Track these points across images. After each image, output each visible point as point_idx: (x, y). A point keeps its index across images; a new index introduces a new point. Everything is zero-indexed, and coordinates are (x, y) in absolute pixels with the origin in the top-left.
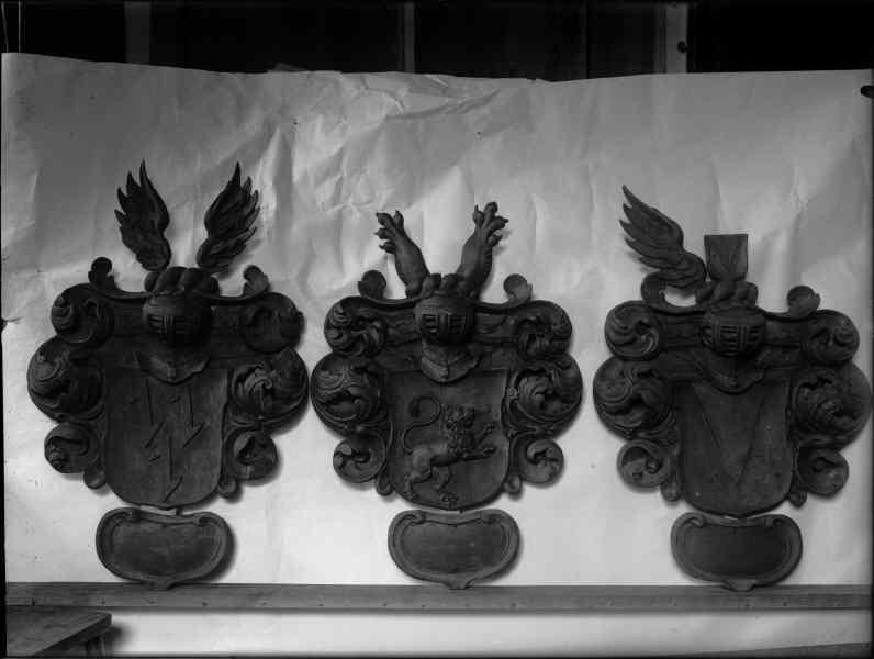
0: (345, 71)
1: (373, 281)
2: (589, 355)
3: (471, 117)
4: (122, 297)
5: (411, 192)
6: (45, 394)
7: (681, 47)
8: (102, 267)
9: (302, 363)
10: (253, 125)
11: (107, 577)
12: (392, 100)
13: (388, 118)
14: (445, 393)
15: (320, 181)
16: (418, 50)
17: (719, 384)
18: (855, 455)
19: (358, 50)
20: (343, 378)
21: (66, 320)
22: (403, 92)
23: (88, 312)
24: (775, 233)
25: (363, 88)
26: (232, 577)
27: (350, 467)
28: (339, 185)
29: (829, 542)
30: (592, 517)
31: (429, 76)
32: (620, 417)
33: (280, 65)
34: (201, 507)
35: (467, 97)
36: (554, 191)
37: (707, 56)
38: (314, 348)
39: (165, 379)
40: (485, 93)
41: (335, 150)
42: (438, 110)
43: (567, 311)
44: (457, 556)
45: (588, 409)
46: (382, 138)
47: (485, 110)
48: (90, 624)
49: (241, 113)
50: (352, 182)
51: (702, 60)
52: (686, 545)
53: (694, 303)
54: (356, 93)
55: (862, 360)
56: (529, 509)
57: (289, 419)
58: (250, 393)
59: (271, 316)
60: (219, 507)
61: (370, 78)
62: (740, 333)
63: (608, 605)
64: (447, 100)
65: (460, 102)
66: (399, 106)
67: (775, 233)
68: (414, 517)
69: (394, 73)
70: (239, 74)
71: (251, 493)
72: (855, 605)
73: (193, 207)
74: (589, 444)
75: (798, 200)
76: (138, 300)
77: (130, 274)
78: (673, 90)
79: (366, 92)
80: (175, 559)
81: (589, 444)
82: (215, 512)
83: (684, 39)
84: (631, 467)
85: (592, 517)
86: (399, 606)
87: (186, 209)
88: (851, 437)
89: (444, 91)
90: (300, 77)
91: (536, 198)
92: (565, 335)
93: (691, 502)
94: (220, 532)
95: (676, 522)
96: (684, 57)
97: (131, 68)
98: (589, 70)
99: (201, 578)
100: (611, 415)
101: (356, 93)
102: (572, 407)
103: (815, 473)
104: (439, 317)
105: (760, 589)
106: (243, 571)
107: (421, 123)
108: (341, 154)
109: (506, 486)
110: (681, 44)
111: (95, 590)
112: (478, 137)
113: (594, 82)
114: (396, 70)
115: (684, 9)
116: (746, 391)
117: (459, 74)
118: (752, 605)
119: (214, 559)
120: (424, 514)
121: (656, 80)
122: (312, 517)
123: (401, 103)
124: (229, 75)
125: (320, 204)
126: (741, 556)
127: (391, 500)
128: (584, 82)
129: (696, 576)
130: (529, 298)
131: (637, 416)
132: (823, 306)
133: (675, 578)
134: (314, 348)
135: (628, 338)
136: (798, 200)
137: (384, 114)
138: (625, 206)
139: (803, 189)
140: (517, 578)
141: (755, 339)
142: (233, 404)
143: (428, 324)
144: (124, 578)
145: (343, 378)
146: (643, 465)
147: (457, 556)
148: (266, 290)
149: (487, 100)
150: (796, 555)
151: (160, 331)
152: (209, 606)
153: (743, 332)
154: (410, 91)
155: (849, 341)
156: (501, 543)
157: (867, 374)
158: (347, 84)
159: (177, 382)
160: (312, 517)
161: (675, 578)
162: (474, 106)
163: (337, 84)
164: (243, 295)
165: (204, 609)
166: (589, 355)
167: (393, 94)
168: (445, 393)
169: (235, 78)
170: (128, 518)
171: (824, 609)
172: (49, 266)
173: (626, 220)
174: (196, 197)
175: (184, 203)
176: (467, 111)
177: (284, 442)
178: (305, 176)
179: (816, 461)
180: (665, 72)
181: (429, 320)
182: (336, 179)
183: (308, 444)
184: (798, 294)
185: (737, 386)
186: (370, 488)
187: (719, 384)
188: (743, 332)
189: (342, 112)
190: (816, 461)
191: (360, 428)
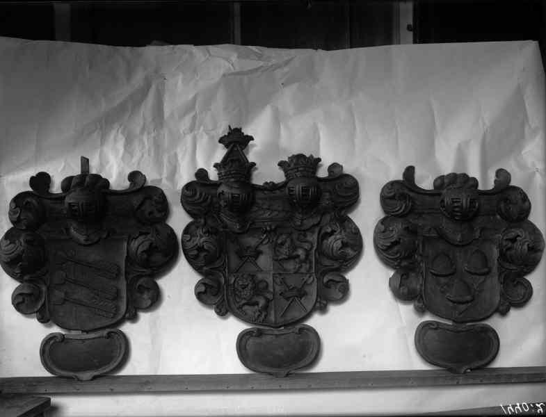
0: (196, 44)
2: (367, 216)
3: (278, 73)
4: (417, 190)
5: (248, 109)
7: (409, 28)
9: (172, 230)
10: (138, 78)
11: (44, 373)
12: (227, 64)
13: (224, 75)
15: (182, 116)
16: (243, 32)
18: (537, 279)
20: (201, 239)
22: (234, 58)
24: (467, 143)
25: (208, 55)
26: (127, 371)
27: (204, 294)
28: (194, 118)
29: (520, 338)
30: (369, 323)
31: (250, 47)
33: (155, 42)
34: (307, 369)
35: (274, 61)
37: (425, 33)
38: (179, 220)
39: (88, 254)
40: (286, 58)
41: (191, 96)
42: (257, 70)
44: (281, 354)
46: (220, 97)
47: (286, 69)
48: (36, 405)
49: (130, 73)
50: (168, 124)
51: (422, 36)
52: (425, 342)
54: (203, 59)
55: (538, 217)
57: (167, 264)
61: (213, 49)
63: (370, 385)
64: (261, 63)
65: (270, 64)
66: (232, 67)
67: (467, 143)
69: (227, 45)
70: (128, 48)
72: (525, 380)
73: (100, 133)
74: (180, 281)
75: (484, 124)
78: (405, 55)
79: (210, 58)
80: (91, 357)
83: (411, 22)
85: (369, 323)
86: (237, 387)
87: (96, 134)
89: (260, 57)
90: (167, 49)
91: (320, 125)
94: (122, 341)
95: (243, 331)
96: (411, 34)
97: (59, 44)
98: (351, 43)
99: (107, 373)
101: (203, 59)
105: (478, 371)
106: (136, 366)
107: (246, 78)
108: (195, 98)
109: (318, 305)
111: (40, 382)
112: (282, 86)
113: (354, 50)
114: (229, 43)
115: (410, 6)
117: (269, 46)
118: (461, 382)
121: (394, 48)
122: (182, 332)
123: (232, 65)
124: (121, 48)
125: (181, 132)
126: (460, 351)
127: (225, 319)
128: (349, 50)
129: (432, 363)
132: (513, 183)
133: (419, 365)
136: (484, 124)
137: (222, 72)
139: (487, 117)
144: (52, 373)
145: (201, 239)
146: (215, 295)
147: (281, 354)
149: (287, 63)
152: (115, 391)
154: (238, 57)
156: (309, 347)
158: (197, 53)
160: (182, 332)
161: (419, 365)
162: (279, 66)
163: (191, 53)
165: (112, 393)
167: (227, 59)
168: (270, 243)
169: (127, 50)
170: (254, 334)
171: (506, 383)
172: (9, 172)
174: (101, 128)
175: (94, 131)
176: (273, 70)
177: (164, 283)
178: (172, 114)
180: (399, 44)
182: (192, 114)
183: (180, 281)
189: (195, 71)
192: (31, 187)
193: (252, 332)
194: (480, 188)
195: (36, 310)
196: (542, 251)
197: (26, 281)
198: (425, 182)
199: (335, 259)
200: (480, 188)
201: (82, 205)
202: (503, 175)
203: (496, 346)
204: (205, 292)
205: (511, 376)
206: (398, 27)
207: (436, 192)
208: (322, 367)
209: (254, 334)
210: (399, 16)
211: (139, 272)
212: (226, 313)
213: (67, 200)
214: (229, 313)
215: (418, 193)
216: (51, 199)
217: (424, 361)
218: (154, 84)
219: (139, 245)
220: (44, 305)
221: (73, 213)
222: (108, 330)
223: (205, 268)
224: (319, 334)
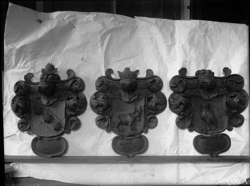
6: (16, 110)
7: (188, 7)
11: (35, 155)
14: (129, 103)
19: (171, 12)
21: (17, 88)
27: (100, 122)
30: (168, 134)
32: (178, 109)
39: (50, 103)
43: (161, 78)
44: (131, 147)
50: (90, 48)
52: (115, 144)
55: (246, 88)
58: (68, 105)
60: (226, 132)
68: (38, 138)
71: (150, 131)
81: (89, 117)
82: (146, 136)
83: (189, 5)
84: (21, 125)
85: (168, 134)
88: (243, 110)
96: (189, 10)
100: (95, 108)
102: (163, 106)
103: (236, 121)
106: (151, 151)
110: (188, 7)
116: (132, 102)
122: (91, 137)
126: (213, 148)
127: (110, 133)
131: (101, 109)
134: (167, 92)
135: (175, 85)
138: (49, 63)
140: (230, 153)
141: (212, 85)
142: (67, 107)
143: (203, 84)
146: (184, 122)
147: (131, 147)
151: (126, 87)
155: (242, 82)
156: (225, 143)
164: (146, 77)
166: (90, 92)
179: (237, 116)
181: (204, 83)
184: (226, 70)
185: (209, 98)
186: (186, 129)
190: (237, 116)
191: (181, 113)
194: (215, 75)
196: (248, 102)
197: (101, 114)
198: (191, 73)
200: (215, 75)
202: (226, 70)
203: (229, 145)
204: (183, 119)
205: (238, 159)
206: (184, 7)
207: (197, 77)
208: (230, 153)
210: (116, 5)
211: (175, 110)
214: (111, 131)
215: (113, 80)
217: (198, 151)
218: (134, 30)
220: (30, 126)
222: (58, 137)
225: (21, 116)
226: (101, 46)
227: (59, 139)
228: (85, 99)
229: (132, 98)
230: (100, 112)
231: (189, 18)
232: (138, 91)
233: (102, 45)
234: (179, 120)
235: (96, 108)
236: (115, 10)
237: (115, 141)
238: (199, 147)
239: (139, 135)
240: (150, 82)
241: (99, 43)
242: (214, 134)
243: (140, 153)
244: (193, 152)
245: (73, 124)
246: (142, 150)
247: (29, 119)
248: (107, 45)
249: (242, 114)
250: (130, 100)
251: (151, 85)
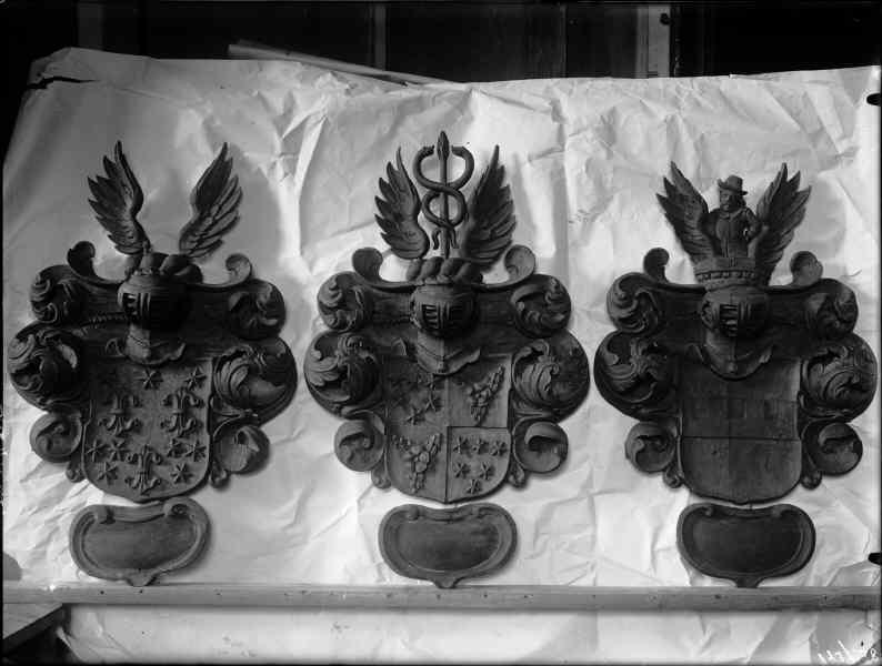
1: (367, 261)
4: (97, 281)
8: (82, 255)
17: (722, 361)
23: (71, 294)
30: (608, 515)
36: (594, 171)
39: (160, 362)
44: (452, 553)
45: (302, 392)
50: (305, 170)
51: (687, 63)
52: (694, 541)
53: (791, 281)
55: (868, 328)
56: (523, 505)
59: (547, 302)
60: (799, 499)
62: (740, 312)
74: (600, 428)
76: (406, 290)
77: (109, 258)
80: (153, 547)
82: (497, 503)
84: (347, 450)
92: (850, 314)
93: (696, 492)
103: (827, 454)
104: (740, 306)
119: (501, 546)
120: (715, 507)
122: (321, 509)
126: (747, 550)
130: (534, 271)
140: (512, 577)
147: (452, 553)
148: (534, 271)
150: (803, 560)
153: (743, 310)
156: (788, 542)
157: (876, 355)
159: (737, 379)
160: (321, 509)
166: (302, 334)
170: (708, 513)
173: (665, 195)
183: (308, 430)
187: (722, 361)
188: (743, 310)
192: (69, 261)
193: (705, 509)
195: (662, 466)
199: (837, 405)
201: (445, 309)
209: (708, 513)
212: (679, 486)
213: (124, 289)
216: (97, 285)
219: (539, 375)
221: (133, 313)
223: (643, 411)
224: (518, 526)
225: (346, 410)
226: (286, 174)
227: (483, 513)
228: (288, 358)
229: (456, 358)
230: (346, 410)
231: (667, 71)
232: (482, 332)
233: (291, 169)
234: (640, 445)
235: (321, 389)
236: (380, 49)
237: (689, 521)
238: (86, 555)
239: (178, 501)
240: (523, 299)
241: (278, 165)
242: (734, 502)
243: (483, 574)
244: (675, 574)
245: (540, 451)
246: (496, 558)
247: (804, 411)
248: (309, 169)
249: (855, 423)
250: (446, 367)
251: (525, 311)
